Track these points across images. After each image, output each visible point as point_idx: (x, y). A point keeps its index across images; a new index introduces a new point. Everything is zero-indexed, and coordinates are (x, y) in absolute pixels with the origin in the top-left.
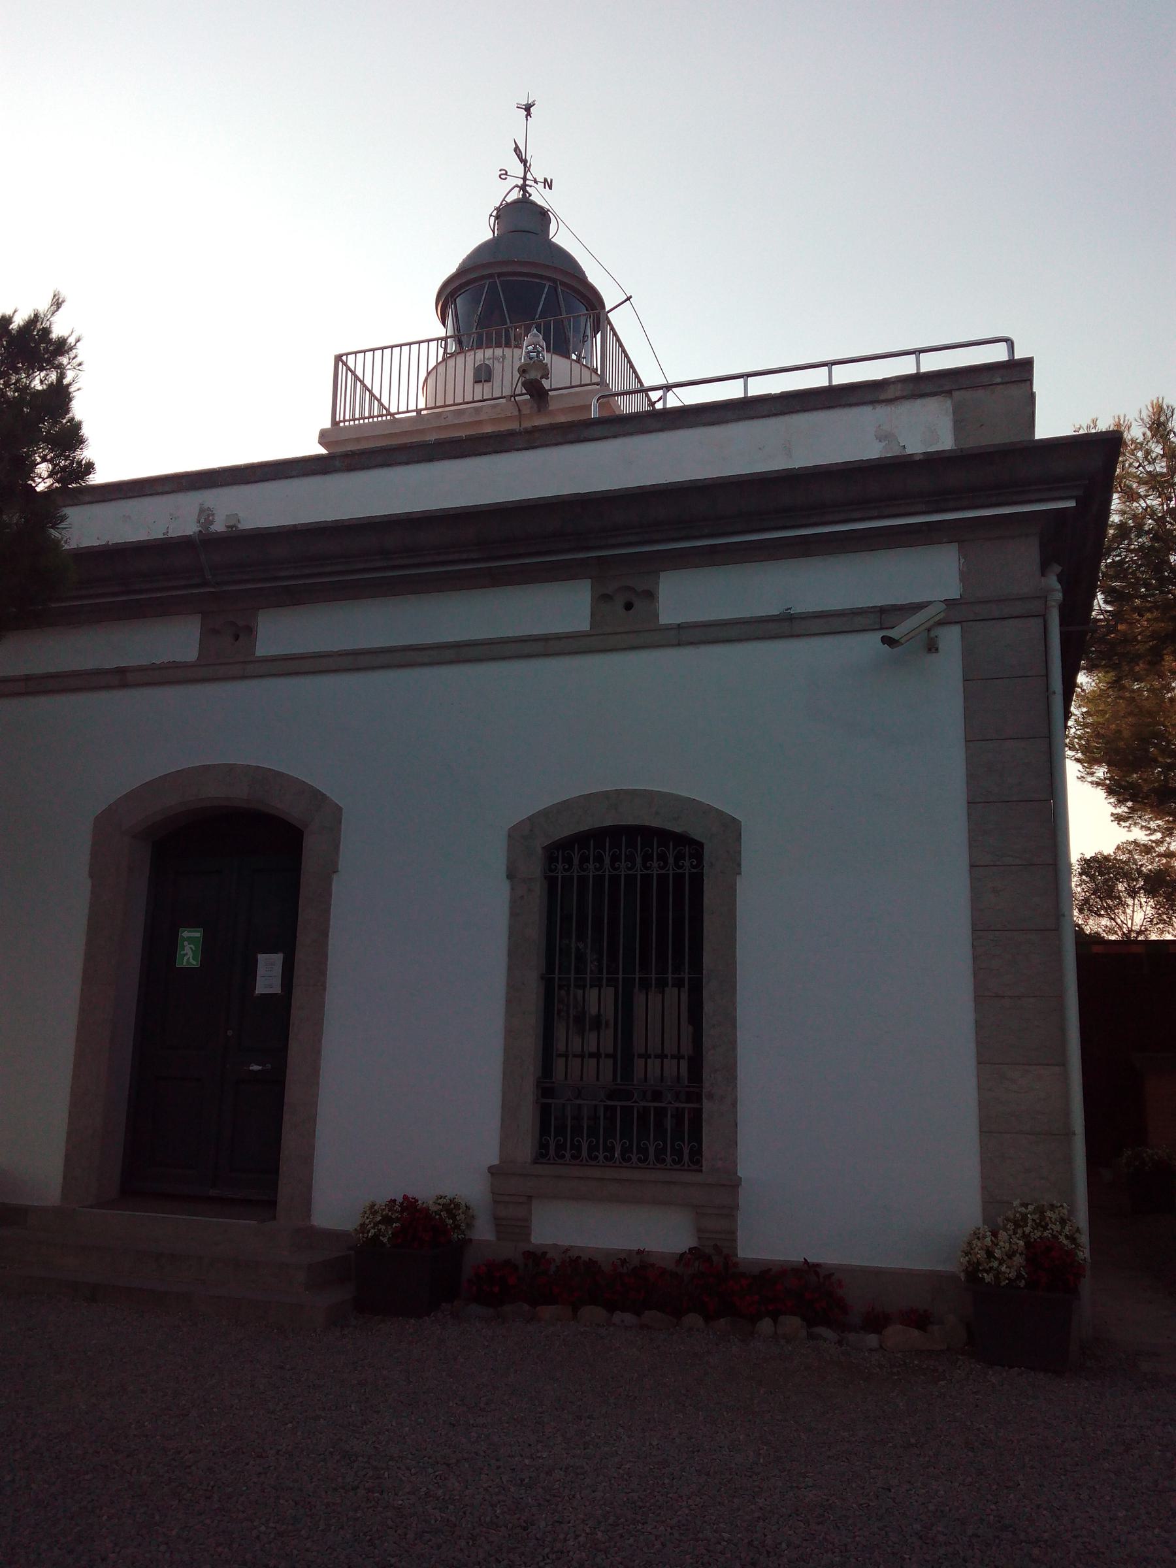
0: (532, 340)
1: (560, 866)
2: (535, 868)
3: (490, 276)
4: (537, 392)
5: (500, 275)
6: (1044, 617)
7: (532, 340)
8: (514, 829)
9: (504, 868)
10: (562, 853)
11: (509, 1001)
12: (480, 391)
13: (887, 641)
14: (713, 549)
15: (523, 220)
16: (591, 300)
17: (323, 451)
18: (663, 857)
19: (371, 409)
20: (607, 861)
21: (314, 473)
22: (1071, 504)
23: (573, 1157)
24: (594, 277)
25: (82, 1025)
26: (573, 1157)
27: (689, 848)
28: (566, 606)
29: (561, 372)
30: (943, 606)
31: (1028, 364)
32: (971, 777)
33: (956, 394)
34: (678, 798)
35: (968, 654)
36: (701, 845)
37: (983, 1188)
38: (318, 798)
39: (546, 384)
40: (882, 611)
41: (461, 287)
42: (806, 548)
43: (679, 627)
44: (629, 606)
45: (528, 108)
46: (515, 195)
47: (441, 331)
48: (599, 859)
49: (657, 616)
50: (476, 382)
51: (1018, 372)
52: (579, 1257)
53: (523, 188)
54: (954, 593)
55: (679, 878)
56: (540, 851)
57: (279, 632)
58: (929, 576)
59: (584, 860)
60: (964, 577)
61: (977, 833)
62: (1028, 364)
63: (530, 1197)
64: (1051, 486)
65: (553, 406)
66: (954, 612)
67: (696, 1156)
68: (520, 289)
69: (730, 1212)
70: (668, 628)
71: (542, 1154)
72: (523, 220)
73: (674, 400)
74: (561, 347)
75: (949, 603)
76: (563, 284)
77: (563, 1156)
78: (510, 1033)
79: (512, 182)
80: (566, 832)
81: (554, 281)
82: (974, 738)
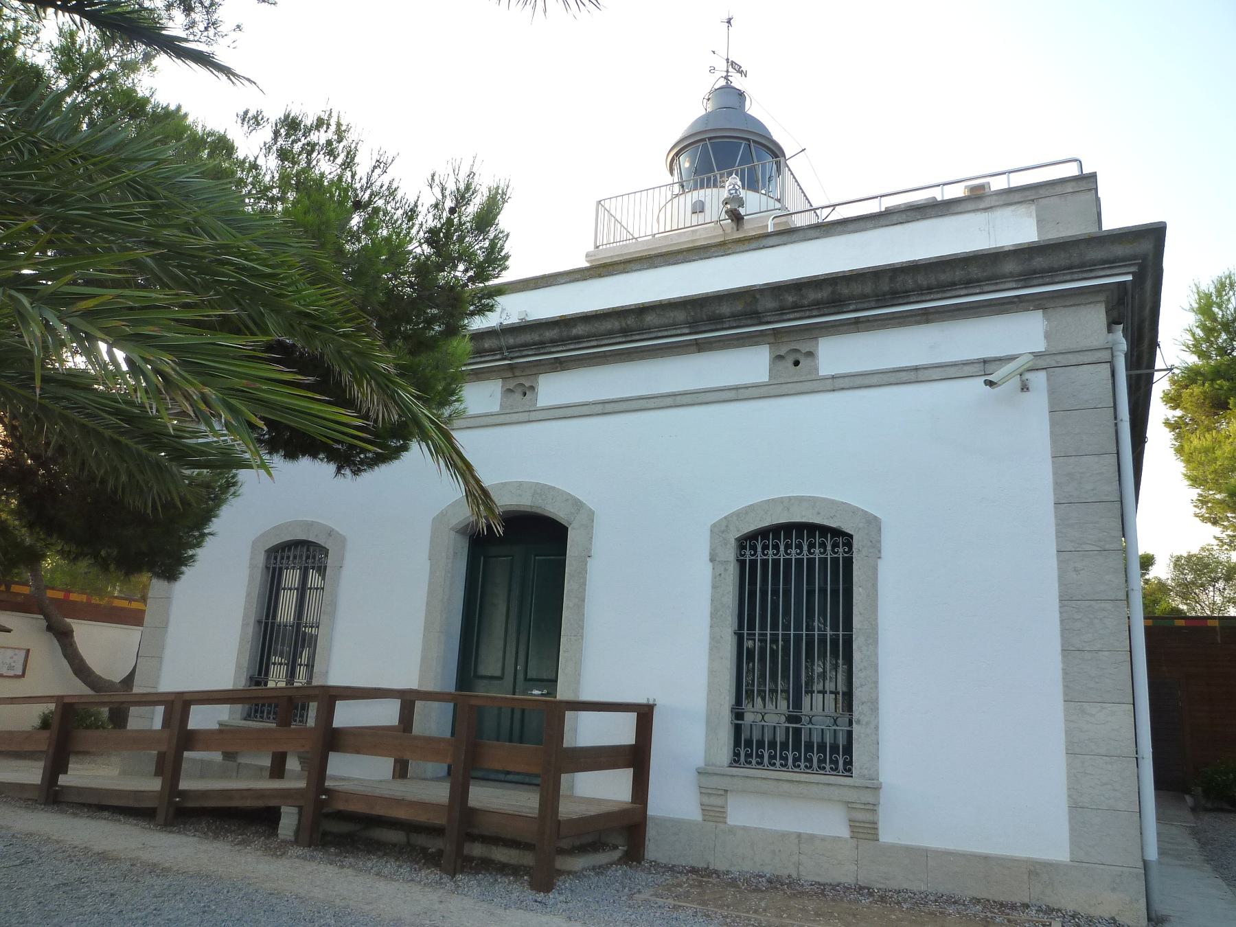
0: (734, 181)
1: (748, 553)
2: (261, 559)
3: (704, 140)
4: (736, 218)
5: (710, 139)
6: (1112, 363)
7: (734, 181)
8: (714, 526)
9: (1063, 747)
10: (747, 541)
11: (711, 649)
12: (696, 219)
13: (990, 384)
14: (857, 321)
15: (730, 98)
16: (775, 152)
17: (587, 265)
18: (823, 545)
19: (625, 235)
20: (782, 548)
21: (592, 277)
22: (1130, 278)
23: (758, 763)
24: (777, 136)
25: (423, 659)
26: (758, 763)
27: (842, 538)
28: (752, 364)
29: (753, 202)
30: (1031, 357)
31: (1093, 176)
32: (1057, 485)
33: (1043, 202)
34: (833, 502)
35: (1052, 392)
36: (851, 536)
37: (1069, 796)
38: (578, 504)
39: (742, 211)
40: (985, 361)
41: (677, 154)
42: (926, 317)
43: (833, 377)
44: (797, 363)
45: (729, 22)
46: (722, 83)
47: (669, 179)
48: (776, 547)
49: (817, 370)
50: (694, 213)
51: (1087, 182)
52: (146, 101)
53: (726, 78)
54: (1041, 346)
55: (835, 561)
56: (733, 541)
57: (554, 389)
58: (1022, 334)
59: (765, 547)
60: (1047, 336)
61: (1063, 525)
62: (1093, 176)
63: (726, 791)
64: (1110, 264)
65: (747, 226)
66: (1039, 362)
67: (849, 764)
68: (729, 146)
69: (872, 808)
70: (825, 378)
71: (736, 761)
72: (730, 98)
73: (836, 216)
74: (752, 184)
75: (1037, 355)
76: (754, 141)
77: (750, 763)
78: (712, 673)
79: (718, 74)
80: (752, 527)
81: (748, 140)
82: (1059, 456)
